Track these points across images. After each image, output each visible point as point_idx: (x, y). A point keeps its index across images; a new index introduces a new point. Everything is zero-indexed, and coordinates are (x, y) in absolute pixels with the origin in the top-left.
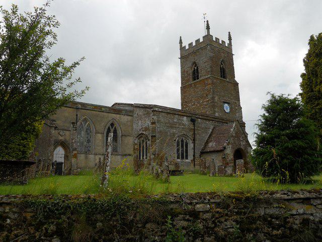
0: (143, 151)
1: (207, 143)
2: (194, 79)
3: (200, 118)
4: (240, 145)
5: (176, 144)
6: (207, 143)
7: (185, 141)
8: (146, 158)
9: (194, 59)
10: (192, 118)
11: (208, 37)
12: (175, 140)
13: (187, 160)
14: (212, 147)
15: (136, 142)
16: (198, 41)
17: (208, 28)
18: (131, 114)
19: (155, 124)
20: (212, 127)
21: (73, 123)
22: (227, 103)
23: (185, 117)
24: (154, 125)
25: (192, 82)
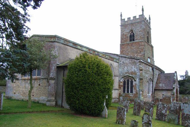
2: (131, 41)
8: (132, 92)
9: (132, 28)
11: (142, 16)
15: (121, 81)
16: (135, 17)
17: (143, 10)
25: (128, 42)
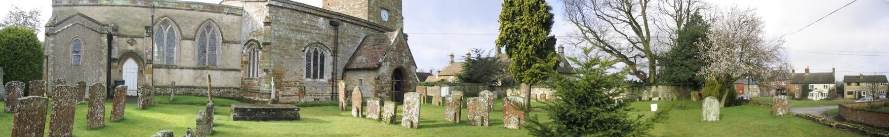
0: (254, 67)
1: (354, 56)
3: (346, 22)
4: (402, 62)
5: (305, 57)
6: (354, 56)
7: (319, 53)
10: (333, 20)
12: (304, 51)
13: (322, 80)
14: (361, 63)
18: (238, 12)
19: (270, 25)
20: (363, 35)
21: (147, 28)
22: (388, 10)
23: (322, 19)
24: (268, 27)
